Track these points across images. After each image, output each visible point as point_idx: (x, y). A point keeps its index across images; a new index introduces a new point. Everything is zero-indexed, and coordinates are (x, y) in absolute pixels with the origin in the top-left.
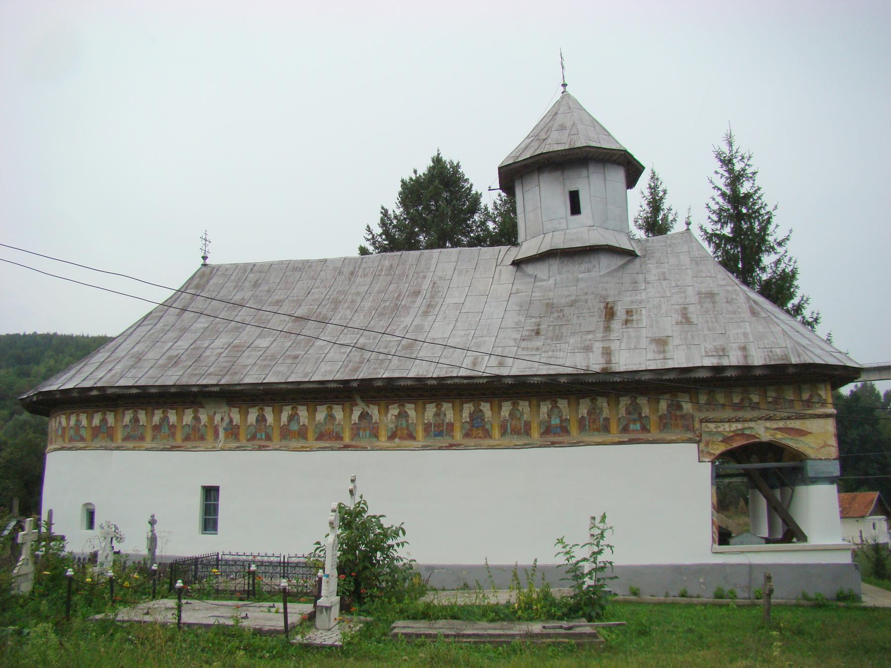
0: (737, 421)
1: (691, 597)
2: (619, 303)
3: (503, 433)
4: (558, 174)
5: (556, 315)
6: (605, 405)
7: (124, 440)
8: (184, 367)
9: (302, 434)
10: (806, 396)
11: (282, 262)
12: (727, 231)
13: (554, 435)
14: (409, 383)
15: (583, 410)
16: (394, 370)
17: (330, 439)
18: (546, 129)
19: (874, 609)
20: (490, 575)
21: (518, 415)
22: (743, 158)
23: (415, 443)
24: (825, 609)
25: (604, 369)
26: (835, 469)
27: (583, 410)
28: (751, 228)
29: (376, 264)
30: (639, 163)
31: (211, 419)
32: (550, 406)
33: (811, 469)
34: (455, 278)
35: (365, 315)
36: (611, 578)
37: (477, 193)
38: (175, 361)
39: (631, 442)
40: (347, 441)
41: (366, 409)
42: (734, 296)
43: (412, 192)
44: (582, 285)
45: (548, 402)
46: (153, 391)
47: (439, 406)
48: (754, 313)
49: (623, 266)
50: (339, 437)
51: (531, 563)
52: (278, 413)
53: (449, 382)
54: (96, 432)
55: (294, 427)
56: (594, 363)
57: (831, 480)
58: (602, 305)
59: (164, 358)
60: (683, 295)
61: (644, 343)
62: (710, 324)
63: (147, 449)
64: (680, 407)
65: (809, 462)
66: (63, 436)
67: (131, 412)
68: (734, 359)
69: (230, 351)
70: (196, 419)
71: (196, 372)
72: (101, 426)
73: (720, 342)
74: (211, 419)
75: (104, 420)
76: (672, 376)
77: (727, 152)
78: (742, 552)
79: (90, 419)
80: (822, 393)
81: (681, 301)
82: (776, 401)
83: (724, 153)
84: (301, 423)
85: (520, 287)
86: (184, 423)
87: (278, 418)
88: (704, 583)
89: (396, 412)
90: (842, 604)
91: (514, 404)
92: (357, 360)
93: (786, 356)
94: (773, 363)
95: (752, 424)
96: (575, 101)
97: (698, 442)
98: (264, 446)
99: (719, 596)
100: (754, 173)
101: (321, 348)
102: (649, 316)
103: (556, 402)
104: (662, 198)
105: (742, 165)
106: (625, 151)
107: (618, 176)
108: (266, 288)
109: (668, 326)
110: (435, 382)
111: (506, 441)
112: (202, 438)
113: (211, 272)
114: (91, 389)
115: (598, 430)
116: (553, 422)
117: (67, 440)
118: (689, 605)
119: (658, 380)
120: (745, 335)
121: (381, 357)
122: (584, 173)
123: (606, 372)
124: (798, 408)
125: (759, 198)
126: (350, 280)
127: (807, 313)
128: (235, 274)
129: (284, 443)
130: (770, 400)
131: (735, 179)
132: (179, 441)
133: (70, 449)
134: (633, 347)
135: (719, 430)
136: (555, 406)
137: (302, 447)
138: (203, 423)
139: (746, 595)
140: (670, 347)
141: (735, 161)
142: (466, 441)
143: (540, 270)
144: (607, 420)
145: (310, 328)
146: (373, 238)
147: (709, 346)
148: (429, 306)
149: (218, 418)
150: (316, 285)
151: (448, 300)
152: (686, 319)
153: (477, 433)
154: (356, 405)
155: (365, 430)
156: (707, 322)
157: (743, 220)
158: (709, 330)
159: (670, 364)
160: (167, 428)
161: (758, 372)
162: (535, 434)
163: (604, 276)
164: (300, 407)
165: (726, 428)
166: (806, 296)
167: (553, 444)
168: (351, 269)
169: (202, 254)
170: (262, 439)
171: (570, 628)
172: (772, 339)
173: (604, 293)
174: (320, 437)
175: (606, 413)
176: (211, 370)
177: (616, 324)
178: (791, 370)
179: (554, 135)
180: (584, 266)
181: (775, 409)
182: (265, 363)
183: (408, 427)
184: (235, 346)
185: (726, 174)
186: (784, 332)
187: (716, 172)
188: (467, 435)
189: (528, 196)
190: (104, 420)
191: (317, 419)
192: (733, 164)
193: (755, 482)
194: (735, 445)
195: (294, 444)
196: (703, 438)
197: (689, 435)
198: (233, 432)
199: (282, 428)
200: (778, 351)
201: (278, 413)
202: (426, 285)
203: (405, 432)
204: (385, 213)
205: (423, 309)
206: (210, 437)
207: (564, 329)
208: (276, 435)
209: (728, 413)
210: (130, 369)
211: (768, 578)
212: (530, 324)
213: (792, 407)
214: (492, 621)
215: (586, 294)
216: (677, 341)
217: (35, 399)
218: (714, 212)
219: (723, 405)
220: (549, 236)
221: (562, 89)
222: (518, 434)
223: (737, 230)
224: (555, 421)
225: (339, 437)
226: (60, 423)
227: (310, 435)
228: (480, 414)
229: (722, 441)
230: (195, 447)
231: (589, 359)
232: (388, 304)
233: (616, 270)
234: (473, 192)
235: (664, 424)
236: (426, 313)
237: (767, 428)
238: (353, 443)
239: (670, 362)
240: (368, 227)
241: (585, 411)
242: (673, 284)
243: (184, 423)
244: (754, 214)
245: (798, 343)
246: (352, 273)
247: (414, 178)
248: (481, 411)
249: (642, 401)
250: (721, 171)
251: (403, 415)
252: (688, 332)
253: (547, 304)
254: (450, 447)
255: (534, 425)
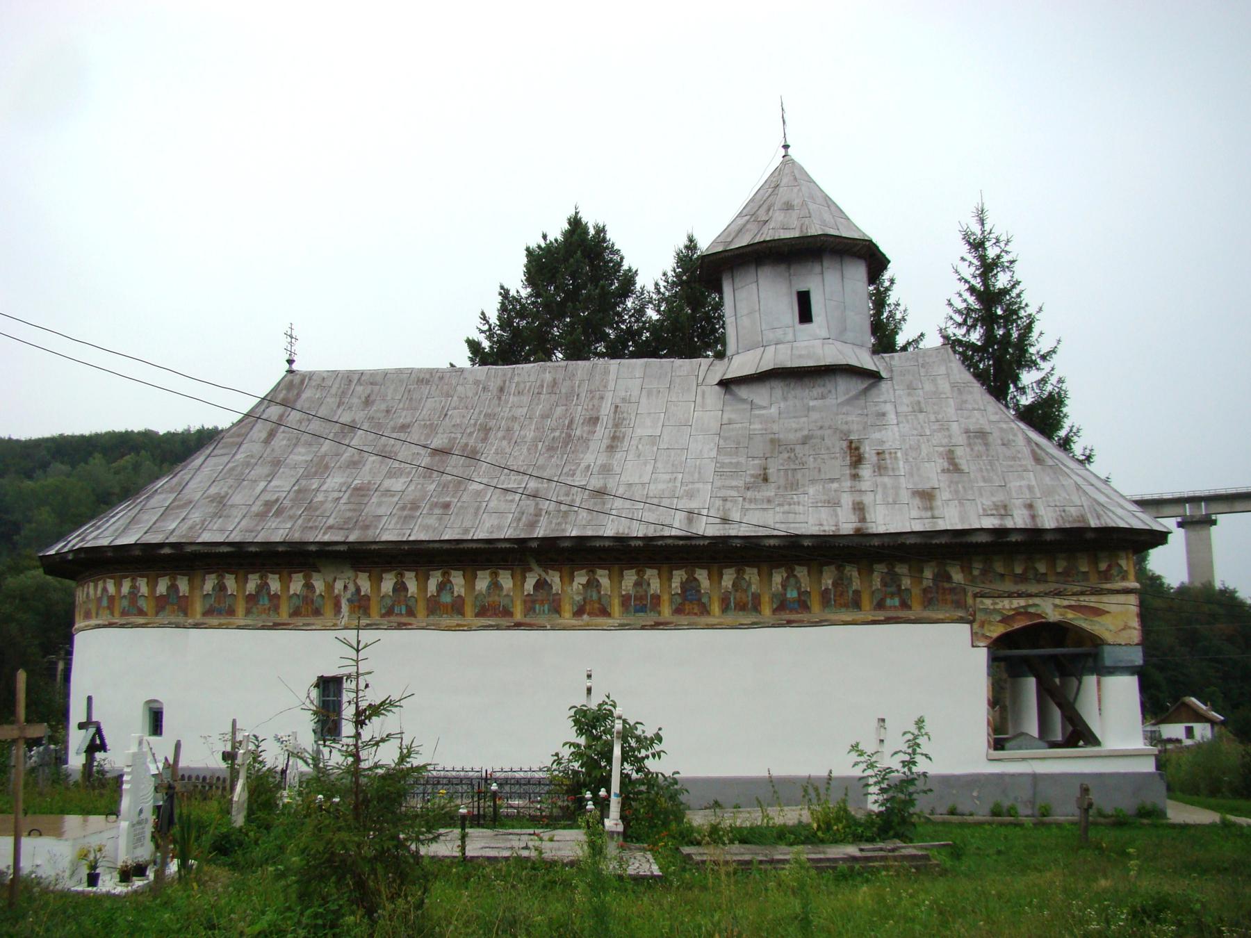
0: (1020, 596)
1: (963, 815)
2: (867, 442)
3: (725, 608)
4: (782, 268)
5: (786, 455)
6: (855, 574)
7: (205, 614)
8: (291, 517)
9: (457, 608)
10: (1103, 566)
11: (399, 371)
12: (976, 337)
13: (791, 611)
14: (607, 544)
15: (828, 581)
16: (584, 526)
17: (495, 615)
18: (765, 207)
19: (1184, 827)
20: (774, 790)
21: (744, 585)
22: (998, 241)
23: (610, 621)
24: (1104, 827)
25: (858, 530)
26: (1137, 658)
27: (828, 581)
28: (1008, 334)
29: (532, 378)
30: (884, 255)
31: (330, 587)
32: (785, 575)
33: (1110, 656)
34: (644, 400)
35: (529, 449)
36: (925, 792)
37: (630, 270)
38: (272, 508)
39: (888, 621)
40: (518, 617)
41: (544, 575)
42: (1011, 437)
43: (542, 265)
44: (815, 416)
45: (783, 569)
46: (252, 549)
47: (640, 573)
48: (1038, 460)
49: (866, 391)
50: (507, 613)
51: (825, 774)
52: (423, 581)
53: (660, 543)
54: (161, 604)
55: (446, 598)
56: (847, 525)
57: (1130, 670)
58: (845, 444)
59: (259, 503)
60: (946, 433)
61: (905, 496)
62: (985, 474)
63: (239, 628)
64: (949, 578)
65: (1107, 649)
66: (111, 608)
67: (213, 576)
68: (1019, 520)
69: (351, 495)
70: (309, 586)
71: (310, 524)
72: (168, 594)
73: (999, 497)
74: (330, 587)
75: (173, 588)
76: (943, 540)
77: (979, 233)
78: (1024, 759)
79: (152, 585)
80: (1123, 563)
81: (945, 441)
82: (1066, 573)
83: (973, 234)
84: (456, 594)
85: (733, 416)
86: (292, 592)
87: (423, 587)
88: (978, 798)
89: (584, 580)
90: (1145, 821)
91: (738, 572)
92: (532, 510)
93: (1083, 518)
94: (1068, 526)
95: (1037, 601)
96: (801, 169)
97: (971, 622)
98: (405, 624)
99: (995, 813)
100: (1012, 262)
101: (478, 493)
102: (907, 461)
103: (793, 570)
104: (887, 289)
105: (996, 251)
106: (871, 241)
107: (857, 272)
108: (383, 407)
109: (933, 474)
110: (640, 543)
111: (729, 619)
112: (317, 612)
113: (302, 382)
114: (161, 545)
115: (846, 606)
116: (789, 596)
117: (117, 613)
118: (962, 825)
119: (926, 544)
120: (1030, 488)
121: (563, 508)
122: (817, 268)
123: (860, 534)
124: (1094, 581)
125: (1019, 296)
126: (500, 398)
127: (1078, 448)
128: (336, 385)
129: (432, 619)
130: (1059, 570)
131: (988, 268)
132: (284, 616)
133: (122, 626)
134: (891, 500)
135: (998, 607)
136: (791, 574)
137: (458, 625)
138: (318, 592)
139: (1029, 812)
140: (938, 503)
141: (987, 244)
142: (675, 619)
143: (759, 395)
144: (857, 592)
145: (455, 464)
146: (490, 329)
147: (988, 503)
148: (614, 438)
149: (339, 586)
150: (453, 405)
151: (639, 432)
152: (953, 467)
153: (691, 609)
154: (531, 570)
155: (542, 603)
156: (981, 470)
157: (997, 323)
158: (985, 480)
159: (942, 525)
160: (266, 598)
161: (1049, 537)
162: (767, 610)
163: (842, 404)
164: (453, 573)
165: (1006, 604)
166: (1076, 425)
167: (789, 623)
168: (499, 382)
169: (287, 357)
170: (401, 614)
171: (893, 850)
172: (1064, 495)
173: (845, 427)
174: (482, 612)
175: (856, 584)
176: (331, 521)
177: (866, 471)
178: (1089, 535)
179: (778, 217)
180: (816, 391)
181: (1066, 582)
182: (405, 513)
183: (600, 599)
184: (356, 489)
185: (977, 263)
186: (1078, 487)
187: (963, 259)
188: (678, 611)
189: (742, 294)
190: (173, 588)
191: (478, 587)
192: (985, 249)
193: (1038, 669)
194: (1017, 626)
195: (447, 621)
196: (978, 617)
197: (960, 614)
198: (361, 605)
199: (428, 600)
200: (1073, 511)
201: (423, 581)
202: (606, 409)
203: (597, 606)
204: (505, 293)
205: (606, 442)
206: (328, 610)
207: (799, 476)
208: (421, 609)
209: (1009, 586)
210: (212, 517)
211: (1085, 791)
212: (753, 467)
213: (1087, 580)
214: (791, 844)
215: (821, 428)
216: (946, 495)
217: (70, 557)
218: (959, 312)
219: (1002, 575)
220: (771, 350)
221: (783, 152)
222: (742, 609)
223: (989, 337)
224: (792, 594)
225: (507, 613)
226: (105, 590)
227: (469, 609)
228: (694, 584)
229: (1000, 621)
230: (308, 625)
231: (837, 516)
232: (557, 434)
233: (856, 397)
234: (625, 267)
235: (929, 600)
236: (611, 448)
237: (1056, 606)
238: (527, 620)
239: (940, 522)
240: (483, 313)
241: (830, 582)
242: (933, 418)
243: (292, 592)
244: (1012, 314)
245: (1095, 500)
246: (501, 390)
247: (543, 245)
248: (696, 579)
249: (901, 569)
250: (970, 257)
251: (592, 584)
252: (957, 483)
253: (772, 441)
254: (656, 626)
255: (765, 599)
